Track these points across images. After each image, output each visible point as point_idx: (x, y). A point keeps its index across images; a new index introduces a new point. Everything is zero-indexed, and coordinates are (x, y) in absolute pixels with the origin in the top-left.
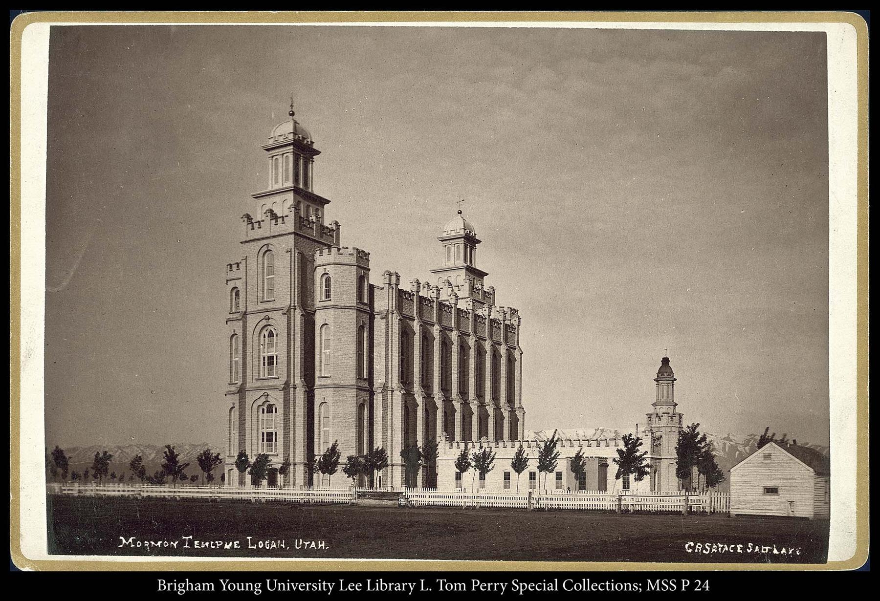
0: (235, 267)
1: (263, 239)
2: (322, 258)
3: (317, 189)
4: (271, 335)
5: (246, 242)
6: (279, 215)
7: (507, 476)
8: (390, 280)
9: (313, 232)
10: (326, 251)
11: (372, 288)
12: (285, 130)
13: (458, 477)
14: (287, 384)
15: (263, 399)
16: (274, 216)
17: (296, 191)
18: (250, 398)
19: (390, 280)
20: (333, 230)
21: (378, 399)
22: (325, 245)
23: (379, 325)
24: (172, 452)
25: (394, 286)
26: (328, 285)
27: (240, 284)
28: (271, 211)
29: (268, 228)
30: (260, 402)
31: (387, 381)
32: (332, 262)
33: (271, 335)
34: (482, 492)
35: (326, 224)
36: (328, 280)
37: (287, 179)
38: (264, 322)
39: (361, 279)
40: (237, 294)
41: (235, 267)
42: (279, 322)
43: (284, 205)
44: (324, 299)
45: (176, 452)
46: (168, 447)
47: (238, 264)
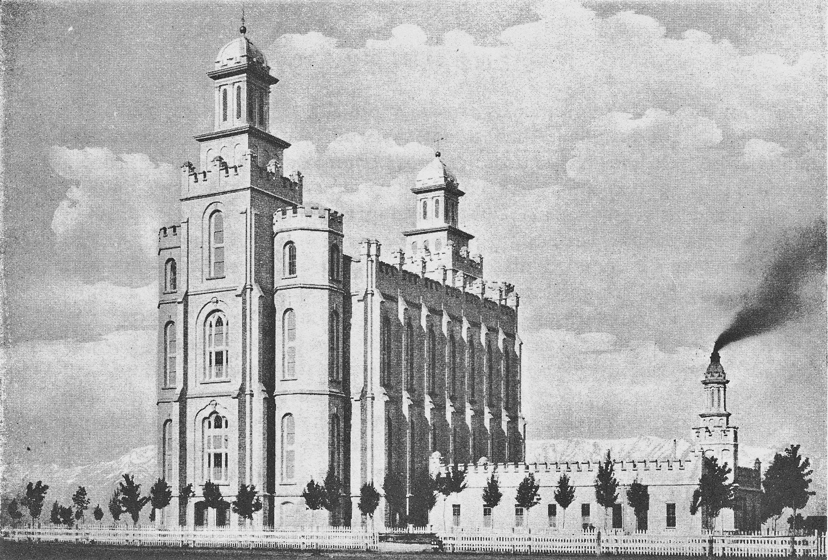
0: (170, 231)
1: (209, 196)
2: (285, 223)
3: (274, 130)
4: (219, 322)
5: (187, 199)
6: (230, 165)
7: (552, 511)
8: (369, 251)
9: (275, 192)
10: (290, 212)
11: (348, 260)
12: (232, 53)
13: (487, 512)
14: (242, 389)
15: (210, 409)
16: (225, 166)
17: (252, 132)
18: (192, 407)
19: (369, 251)
20: (296, 183)
21: (356, 407)
22: (291, 204)
23: (357, 308)
24: (130, 483)
25: (374, 258)
26: (293, 257)
27: (174, 254)
28: (221, 159)
29: (217, 180)
30: (206, 413)
31: (366, 386)
32: (299, 226)
33: (219, 322)
34: (484, 532)
35: (286, 175)
36: (293, 251)
37: (239, 116)
38: (211, 307)
39: (334, 249)
40: (174, 268)
41: (170, 231)
42: (232, 309)
43: (239, 150)
44: (287, 275)
45: (136, 483)
46: (126, 477)
47: (174, 228)
